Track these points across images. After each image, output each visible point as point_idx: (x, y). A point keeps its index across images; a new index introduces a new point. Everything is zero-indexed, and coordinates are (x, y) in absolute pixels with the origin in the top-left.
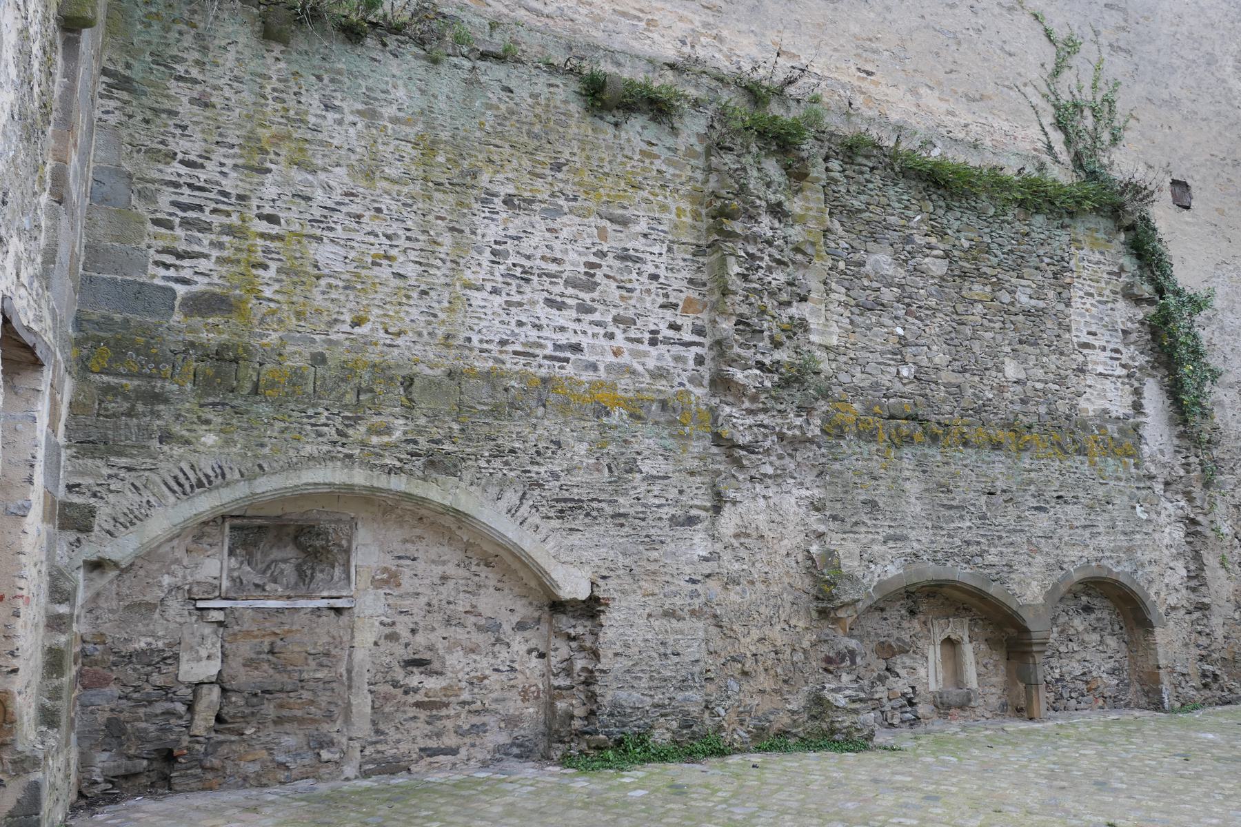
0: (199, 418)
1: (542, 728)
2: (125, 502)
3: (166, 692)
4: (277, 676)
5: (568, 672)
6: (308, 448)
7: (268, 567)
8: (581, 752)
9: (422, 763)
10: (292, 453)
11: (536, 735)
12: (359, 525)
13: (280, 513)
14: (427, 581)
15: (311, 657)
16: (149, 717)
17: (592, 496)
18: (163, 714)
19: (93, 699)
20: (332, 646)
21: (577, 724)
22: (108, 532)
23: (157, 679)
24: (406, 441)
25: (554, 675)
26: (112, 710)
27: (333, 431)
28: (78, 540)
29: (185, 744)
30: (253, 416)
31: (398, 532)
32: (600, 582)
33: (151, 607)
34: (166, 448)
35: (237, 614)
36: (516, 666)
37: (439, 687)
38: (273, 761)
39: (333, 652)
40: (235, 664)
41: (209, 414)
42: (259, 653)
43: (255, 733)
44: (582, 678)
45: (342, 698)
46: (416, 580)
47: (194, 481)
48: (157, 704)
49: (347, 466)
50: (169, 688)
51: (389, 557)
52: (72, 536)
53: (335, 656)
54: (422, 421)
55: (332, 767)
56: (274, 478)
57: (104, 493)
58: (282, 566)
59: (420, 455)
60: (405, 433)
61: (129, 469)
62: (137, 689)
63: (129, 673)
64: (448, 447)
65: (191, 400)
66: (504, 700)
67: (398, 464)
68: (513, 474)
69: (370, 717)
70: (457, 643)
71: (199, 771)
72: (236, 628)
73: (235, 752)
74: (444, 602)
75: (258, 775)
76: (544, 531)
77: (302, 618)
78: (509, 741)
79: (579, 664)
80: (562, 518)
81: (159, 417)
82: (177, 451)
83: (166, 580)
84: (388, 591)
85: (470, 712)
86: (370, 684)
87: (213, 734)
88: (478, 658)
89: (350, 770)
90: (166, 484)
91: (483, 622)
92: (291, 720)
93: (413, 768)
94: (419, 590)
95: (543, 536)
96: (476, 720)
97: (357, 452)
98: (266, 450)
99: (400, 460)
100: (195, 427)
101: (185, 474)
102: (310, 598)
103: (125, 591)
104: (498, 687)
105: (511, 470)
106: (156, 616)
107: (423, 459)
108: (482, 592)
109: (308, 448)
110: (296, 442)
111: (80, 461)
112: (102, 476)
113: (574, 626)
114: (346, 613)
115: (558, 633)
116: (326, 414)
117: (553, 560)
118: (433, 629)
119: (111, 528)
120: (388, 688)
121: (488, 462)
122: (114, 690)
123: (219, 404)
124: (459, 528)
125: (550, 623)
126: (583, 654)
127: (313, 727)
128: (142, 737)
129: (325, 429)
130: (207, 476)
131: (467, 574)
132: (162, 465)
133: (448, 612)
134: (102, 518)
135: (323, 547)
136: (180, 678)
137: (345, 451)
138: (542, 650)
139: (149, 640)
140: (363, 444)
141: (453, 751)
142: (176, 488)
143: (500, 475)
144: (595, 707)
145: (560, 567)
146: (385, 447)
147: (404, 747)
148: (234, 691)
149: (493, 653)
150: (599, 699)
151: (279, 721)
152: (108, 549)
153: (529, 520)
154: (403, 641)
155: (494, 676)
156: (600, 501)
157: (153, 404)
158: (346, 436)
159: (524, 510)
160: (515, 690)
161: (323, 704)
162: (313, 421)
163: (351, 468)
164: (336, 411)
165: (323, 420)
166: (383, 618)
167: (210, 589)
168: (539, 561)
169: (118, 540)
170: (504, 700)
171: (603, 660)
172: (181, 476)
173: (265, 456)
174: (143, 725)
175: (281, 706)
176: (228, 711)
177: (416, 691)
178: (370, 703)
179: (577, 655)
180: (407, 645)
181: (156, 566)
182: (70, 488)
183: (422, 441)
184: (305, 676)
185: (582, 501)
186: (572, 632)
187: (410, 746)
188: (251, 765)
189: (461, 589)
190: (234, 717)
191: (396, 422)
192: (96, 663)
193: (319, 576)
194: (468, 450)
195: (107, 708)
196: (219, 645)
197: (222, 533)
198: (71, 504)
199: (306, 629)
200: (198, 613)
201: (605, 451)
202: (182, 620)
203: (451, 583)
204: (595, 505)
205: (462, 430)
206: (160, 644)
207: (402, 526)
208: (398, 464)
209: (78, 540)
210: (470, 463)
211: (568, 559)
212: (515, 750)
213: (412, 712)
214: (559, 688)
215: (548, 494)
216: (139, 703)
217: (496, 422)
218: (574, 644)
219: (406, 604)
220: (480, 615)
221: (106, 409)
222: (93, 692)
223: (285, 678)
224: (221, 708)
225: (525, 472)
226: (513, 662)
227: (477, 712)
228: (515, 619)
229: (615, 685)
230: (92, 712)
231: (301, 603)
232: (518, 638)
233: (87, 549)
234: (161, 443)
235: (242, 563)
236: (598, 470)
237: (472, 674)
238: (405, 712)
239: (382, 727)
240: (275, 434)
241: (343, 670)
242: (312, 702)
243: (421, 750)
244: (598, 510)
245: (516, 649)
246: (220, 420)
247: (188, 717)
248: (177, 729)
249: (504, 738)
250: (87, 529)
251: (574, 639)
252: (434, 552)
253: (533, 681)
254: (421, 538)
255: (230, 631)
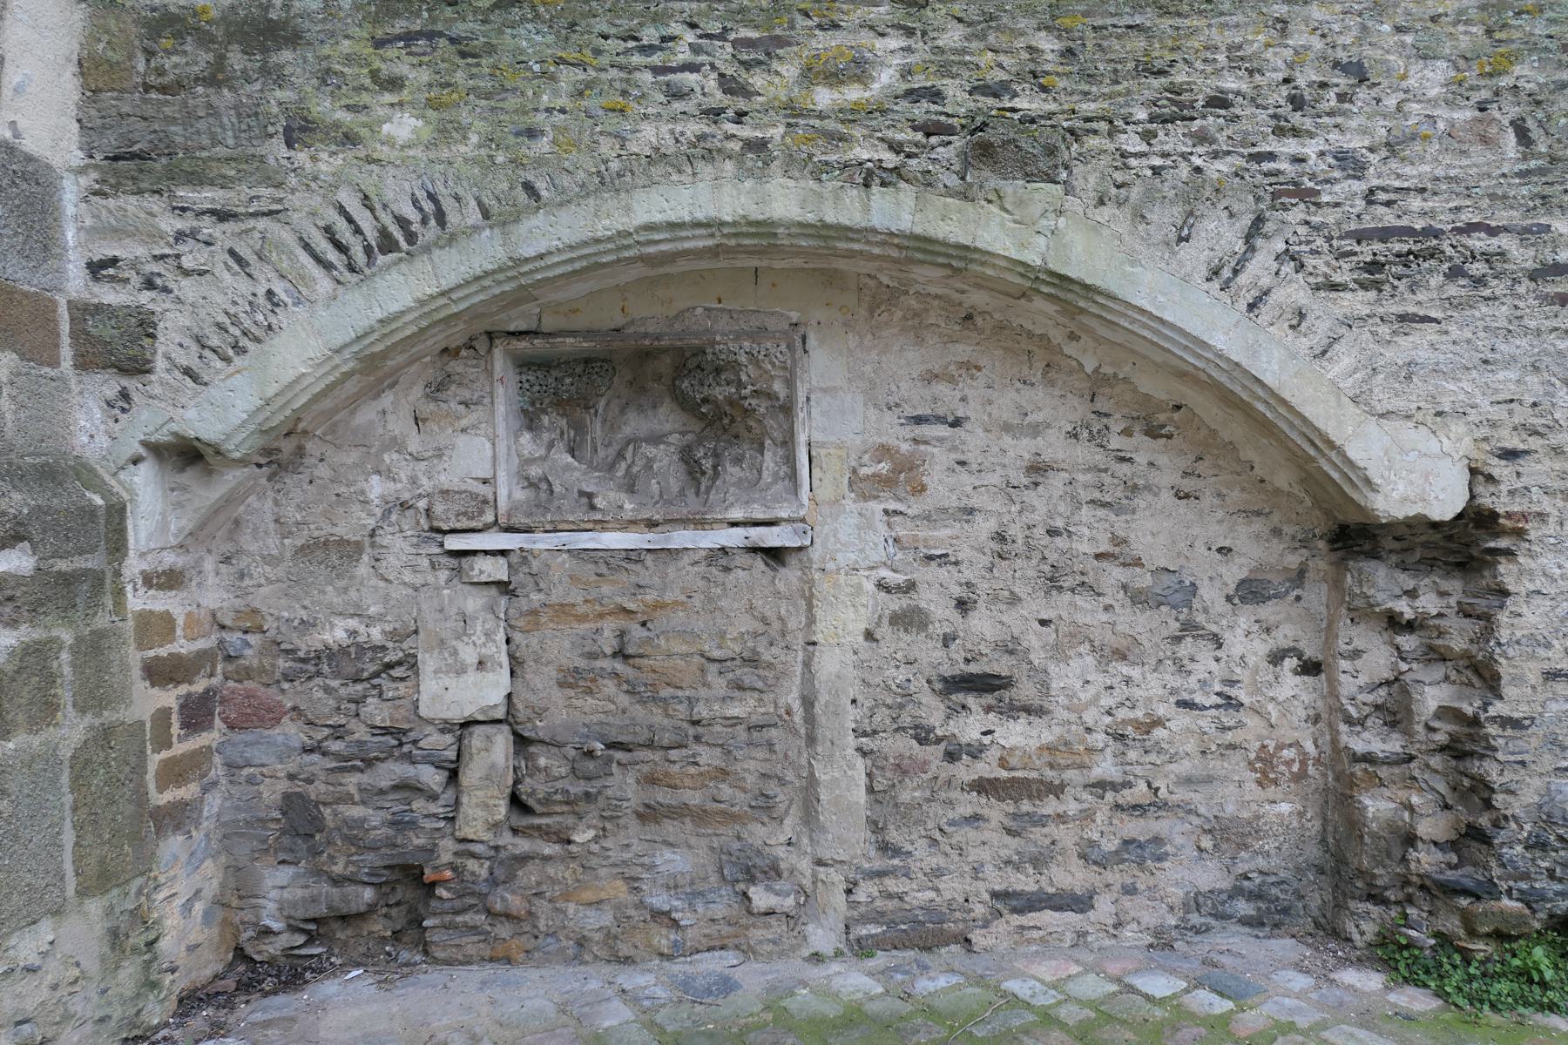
0: (374, 74)
1: (1313, 852)
2: (219, 298)
3: (398, 737)
4: (639, 711)
5: (1395, 715)
6: (649, 132)
7: (620, 455)
8: (1443, 939)
9: (1000, 926)
10: (607, 147)
11: (1298, 869)
12: (812, 342)
13: (619, 320)
14: (994, 479)
15: (714, 668)
16: (371, 795)
17: (1466, 217)
18: (396, 788)
19: (249, 753)
20: (763, 641)
21: (1426, 860)
22: (187, 372)
23: (377, 711)
24: (909, 93)
25: (1349, 721)
26: (291, 777)
27: (712, 83)
28: (125, 395)
29: (446, 857)
30: (506, 60)
31: (912, 354)
32: (1500, 469)
33: (349, 550)
34: (302, 157)
35: (535, 565)
36: (1240, 694)
37: (1034, 744)
38: (641, 905)
39: (766, 657)
40: (541, 681)
41: (397, 62)
42: (592, 656)
43: (596, 839)
44: (1441, 738)
45: (796, 768)
46: (965, 479)
47: (372, 236)
48: (382, 767)
49: (750, 173)
50: (405, 732)
51: (890, 418)
52: (110, 385)
53: (770, 666)
54: (953, 36)
55: (778, 927)
56: (564, 215)
57: (170, 278)
58: (649, 450)
59: (950, 130)
60: (906, 73)
61: (222, 216)
62: (338, 732)
63: (317, 696)
64: (1028, 102)
65: (355, 31)
66: (1209, 780)
67: (890, 159)
68: (1223, 166)
69: (864, 813)
70: (1079, 635)
71: (481, 918)
72: (536, 597)
73: (554, 881)
74: (1039, 531)
75: (610, 937)
76: (1321, 327)
77: (686, 575)
78: (1225, 884)
79: (1432, 696)
80: (1377, 286)
81: (281, 81)
82: (328, 163)
83: (376, 488)
84: (892, 505)
85: (1118, 807)
86: (859, 733)
87: (506, 838)
88: (1135, 673)
89: (822, 937)
90: (307, 247)
91: (1144, 580)
92: (679, 812)
93: (976, 937)
94: (974, 502)
95: (1318, 340)
96: (1134, 828)
97: (777, 132)
98: (543, 145)
99: (895, 148)
100: (365, 98)
101: (350, 220)
102: (700, 523)
103: (292, 514)
104: (1191, 746)
105: (1216, 155)
106: (363, 569)
107: (958, 142)
108: (1140, 502)
109: (649, 132)
110: (614, 119)
111: (111, 202)
112: (162, 235)
113: (1412, 594)
114: (793, 560)
115: (1362, 613)
116: (690, 37)
117: (1351, 409)
118: (1014, 600)
119: (195, 364)
120: (904, 745)
121: (1148, 136)
122: (291, 732)
123: (419, 34)
124: (1073, 337)
125: (1337, 585)
126: (1438, 671)
127: (728, 831)
128: (355, 837)
129: (691, 78)
130: (403, 222)
131: (1099, 458)
132: (296, 200)
133: (1053, 557)
134: (170, 344)
135: (731, 403)
136: (423, 712)
137: (746, 132)
138: (1309, 653)
139: (353, 623)
140: (793, 111)
141: (1079, 903)
142: (332, 255)
143: (1184, 171)
144: (1484, 821)
145: (1372, 426)
146: (851, 114)
147: (952, 887)
148: (542, 742)
149: (1176, 661)
150: (1499, 800)
151: (649, 814)
152: (191, 414)
153: (1277, 296)
154: (938, 629)
155: (1181, 720)
156: (1493, 232)
157: (265, 50)
158: (745, 92)
159: (1260, 267)
160: (1237, 756)
161: (750, 780)
162: (656, 59)
163: (761, 176)
164: (715, 27)
165: (683, 55)
166: (884, 573)
167: (472, 507)
168: (1309, 411)
169: (212, 392)
170: (1209, 780)
171: (1508, 691)
172: (341, 225)
173: (540, 162)
174: (356, 812)
175: (652, 780)
176: (533, 788)
177: (976, 752)
178: (862, 780)
179: (1418, 672)
180: (947, 640)
181: (352, 457)
182: (96, 269)
183: (955, 92)
184: (702, 711)
185: (1437, 234)
186: (1404, 608)
187: (968, 885)
188: (591, 913)
189: (1084, 495)
190: (547, 801)
191: (879, 44)
192: (246, 674)
193: (732, 472)
194: (1088, 108)
195: (281, 769)
196: (500, 637)
197: (490, 373)
198: (99, 309)
199: (697, 601)
200: (453, 562)
201: (1505, 81)
202: (419, 580)
203: (1056, 482)
204: (1478, 242)
205: (1069, 53)
206: (376, 634)
207: (920, 341)
208: (890, 159)
209: (125, 395)
210: (1092, 142)
211: (1399, 404)
212: (1244, 907)
213: (968, 804)
214: (1368, 758)
215: (1330, 217)
216: (346, 765)
217: (1166, 23)
218: (1408, 642)
219: (941, 536)
220: (1138, 562)
221: (161, 72)
222: (247, 737)
223: (658, 717)
224: (517, 782)
225: (1259, 158)
226: (1232, 683)
227: (1138, 809)
228: (1234, 572)
229: (1548, 761)
230: (251, 781)
231: (681, 538)
232: (1245, 620)
233: (145, 415)
234: (289, 145)
235: (551, 445)
236: (1485, 140)
237: (1122, 714)
238: (950, 803)
239: (893, 836)
240: (562, 102)
241: (792, 697)
242: (723, 774)
243: (995, 895)
244: (1487, 257)
245: (1237, 650)
246: (425, 76)
247: (449, 795)
248: (429, 824)
249: (1210, 877)
250: (139, 368)
251: (1410, 627)
252: (1006, 403)
253: (1289, 736)
254: (970, 367)
255: (523, 604)
